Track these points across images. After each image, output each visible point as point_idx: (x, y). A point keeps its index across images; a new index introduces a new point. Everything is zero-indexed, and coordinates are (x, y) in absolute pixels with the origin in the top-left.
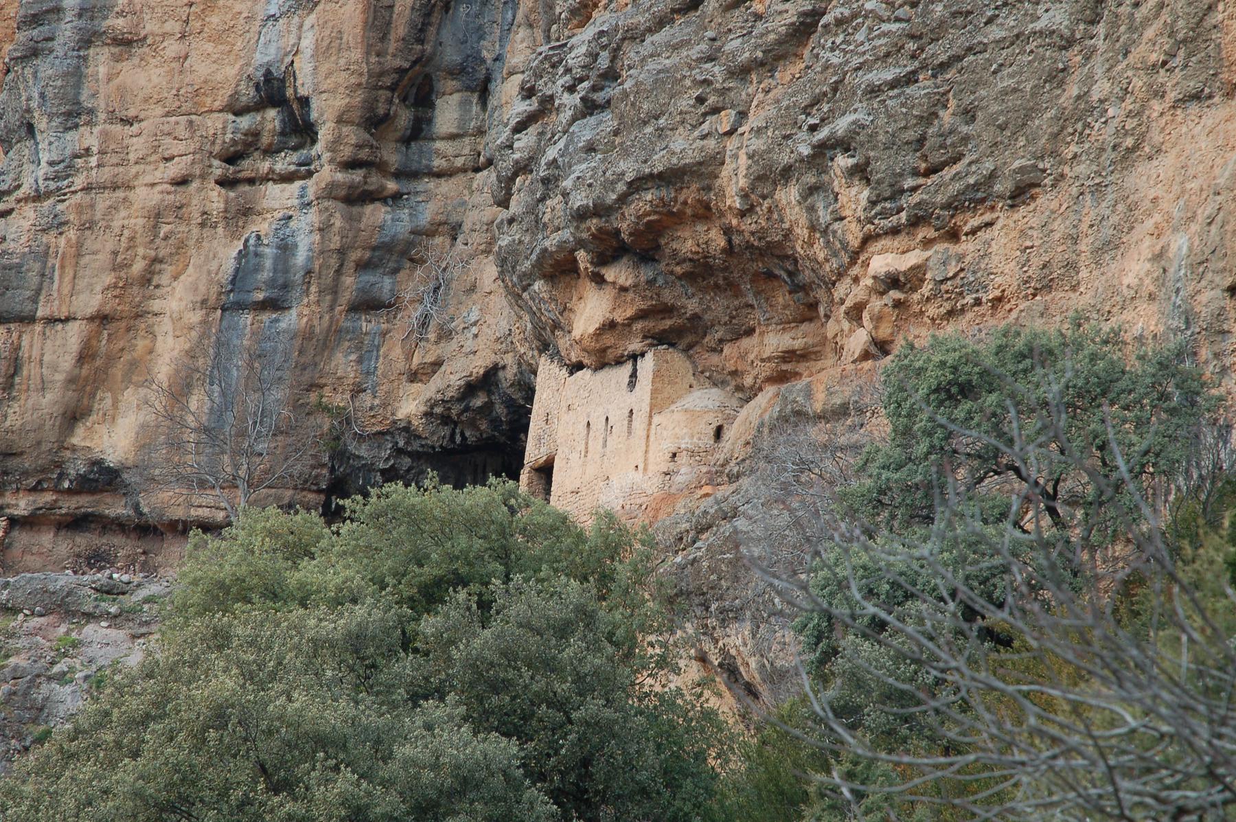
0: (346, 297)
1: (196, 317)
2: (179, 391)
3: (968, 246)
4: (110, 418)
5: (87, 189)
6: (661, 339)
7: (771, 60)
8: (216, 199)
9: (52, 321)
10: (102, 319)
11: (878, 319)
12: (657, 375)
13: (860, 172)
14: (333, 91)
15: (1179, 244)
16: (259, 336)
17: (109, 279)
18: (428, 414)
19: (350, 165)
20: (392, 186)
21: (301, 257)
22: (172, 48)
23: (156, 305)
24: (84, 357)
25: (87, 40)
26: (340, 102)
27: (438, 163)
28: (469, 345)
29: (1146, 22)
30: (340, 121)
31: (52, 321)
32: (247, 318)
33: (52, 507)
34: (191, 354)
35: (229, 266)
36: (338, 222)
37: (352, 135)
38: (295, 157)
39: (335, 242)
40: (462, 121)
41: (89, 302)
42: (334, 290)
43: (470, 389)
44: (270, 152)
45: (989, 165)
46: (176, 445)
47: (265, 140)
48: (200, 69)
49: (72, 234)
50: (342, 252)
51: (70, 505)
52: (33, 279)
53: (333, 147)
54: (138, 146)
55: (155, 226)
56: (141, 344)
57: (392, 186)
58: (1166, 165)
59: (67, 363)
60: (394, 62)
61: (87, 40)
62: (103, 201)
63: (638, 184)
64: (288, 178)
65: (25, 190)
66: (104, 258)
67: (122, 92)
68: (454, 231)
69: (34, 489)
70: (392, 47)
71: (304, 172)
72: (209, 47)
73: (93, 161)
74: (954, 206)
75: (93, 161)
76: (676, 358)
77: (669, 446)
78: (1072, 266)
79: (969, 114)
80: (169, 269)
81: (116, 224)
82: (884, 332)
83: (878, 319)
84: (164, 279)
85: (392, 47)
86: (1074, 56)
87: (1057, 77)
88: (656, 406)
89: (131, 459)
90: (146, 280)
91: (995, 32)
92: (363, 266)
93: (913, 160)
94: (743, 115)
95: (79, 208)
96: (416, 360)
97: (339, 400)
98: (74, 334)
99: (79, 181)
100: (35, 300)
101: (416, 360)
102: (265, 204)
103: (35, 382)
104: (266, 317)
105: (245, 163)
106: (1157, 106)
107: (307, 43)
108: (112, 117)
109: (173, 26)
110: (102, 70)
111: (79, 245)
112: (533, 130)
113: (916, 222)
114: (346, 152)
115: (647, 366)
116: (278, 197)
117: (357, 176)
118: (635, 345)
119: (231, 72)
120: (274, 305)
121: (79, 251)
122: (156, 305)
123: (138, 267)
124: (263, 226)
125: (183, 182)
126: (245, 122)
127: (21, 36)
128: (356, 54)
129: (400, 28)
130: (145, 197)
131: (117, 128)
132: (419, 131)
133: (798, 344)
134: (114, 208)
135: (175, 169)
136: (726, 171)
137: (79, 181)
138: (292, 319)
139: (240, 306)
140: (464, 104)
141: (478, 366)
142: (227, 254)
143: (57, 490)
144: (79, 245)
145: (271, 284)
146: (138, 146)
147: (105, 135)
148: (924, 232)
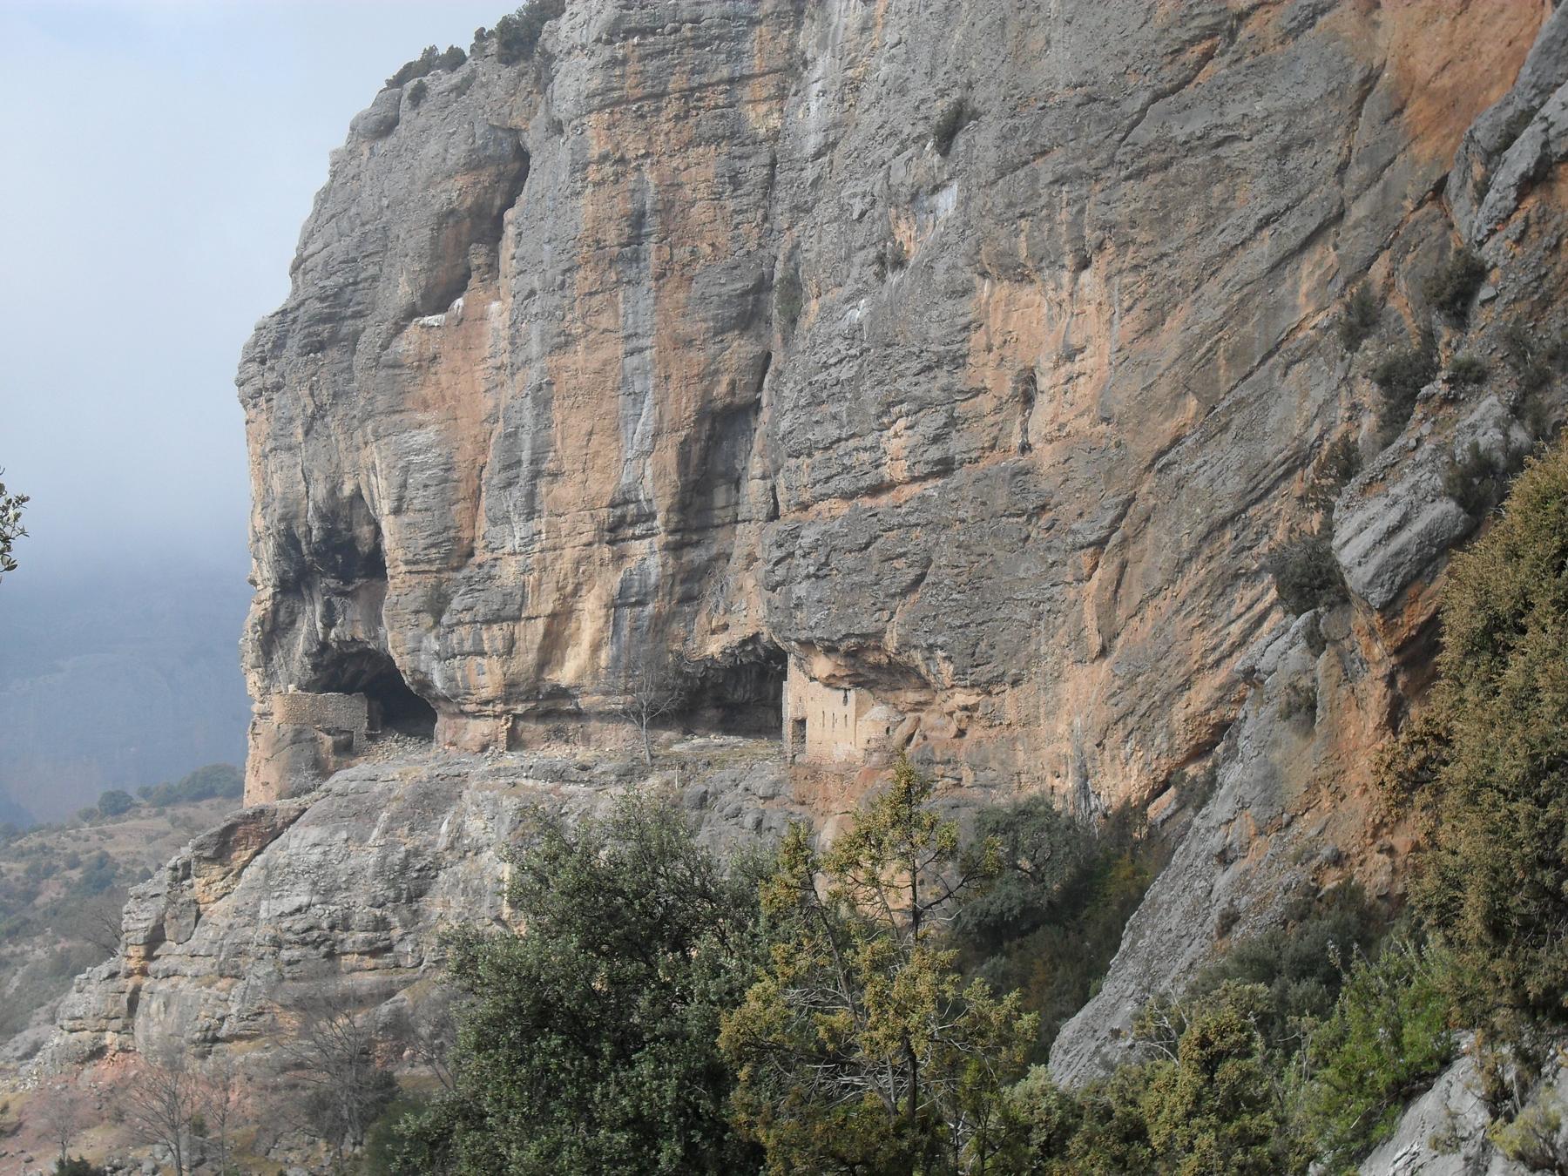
0: (676, 596)
1: (603, 612)
2: (596, 648)
3: (995, 700)
4: (561, 663)
5: (541, 551)
6: (857, 685)
7: (904, 593)
8: (606, 551)
9: (529, 618)
10: (553, 616)
11: (960, 721)
12: (858, 702)
13: (948, 658)
14: (664, 496)
15: (1078, 722)
16: (637, 619)
17: (557, 595)
18: (723, 653)
19: (672, 532)
20: (695, 538)
21: (653, 579)
22: (579, 477)
23: (580, 606)
24: (547, 634)
25: (536, 475)
26: (668, 501)
27: (717, 521)
28: (743, 620)
29: (1059, 627)
30: (668, 511)
31: (529, 618)
32: (627, 611)
33: (533, 709)
34: (601, 631)
35: (617, 586)
36: (671, 561)
37: (674, 518)
38: (645, 526)
39: (670, 571)
40: (728, 501)
41: (548, 608)
42: (671, 594)
43: (744, 643)
44: (633, 524)
45: (1001, 670)
46: (595, 675)
47: (629, 519)
48: (594, 487)
49: (536, 574)
50: (673, 575)
51: (543, 706)
52: (518, 598)
53: (666, 523)
54: (565, 528)
55: (577, 569)
56: (573, 625)
57: (695, 538)
58: (1070, 686)
59: (539, 639)
60: (692, 477)
61: (536, 475)
62: (550, 556)
63: (848, 636)
64: (642, 537)
65: (506, 550)
66: (553, 585)
67: (555, 500)
68: (728, 557)
69: (526, 700)
70: (691, 470)
71: (650, 534)
72: (598, 475)
73: (543, 536)
74: (989, 682)
75: (543, 536)
76: (864, 692)
77: (865, 737)
78: (1037, 718)
79: (992, 647)
80: (585, 588)
81: (557, 567)
82: (963, 726)
83: (960, 721)
84: (583, 592)
85: (691, 470)
86: (1033, 632)
87: (1027, 639)
88: (859, 714)
89: (573, 683)
90: (575, 592)
91: (1000, 615)
92: (683, 582)
93: (969, 661)
94: (893, 614)
95: (538, 561)
96: (714, 624)
97: (676, 647)
98: (540, 625)
99: (537, 547)
100: (520, 610)
101: (714, 624)
102: (631, 552)
103: (523, 649)
104: (637, 609)
105: (620, 531)
106: (1066, 662)
107: (649, 472)
108: (551, 514)
109: (579, 466)
110: (544, 490)
111: (540, 580)
112: (784, 564)
113: (973, 686)
114: (672, 526)
115: (852, 695)
116: (639, 548)
117: (678, 537)
118: (846, 685)
119: (609, 488)
120: (641, 603)
121: (540, 582)
122: (580, 606)
123: (569, 588)
124: (630, 564)
125: (590, 544)
126: (618, 512)
127: (504, 475)
128: (674, 477)
129: (694, 460)
130: (569, 554)
131: (554, 519)
132: (708, 508)
133: (922, 699)
134: (556, 559)
135: (585, 539)
136: (887, 636)
137: (537, 547)
138: (650, 609)
139: (625, 605)
140: (728, 490)
141: (749, 632)
142: (615, 580)
143: (537, 700)
144: (540, 580)
145: (637, 594)
146: (565, 528)
147: (549, 523)
148: (977, 690)
